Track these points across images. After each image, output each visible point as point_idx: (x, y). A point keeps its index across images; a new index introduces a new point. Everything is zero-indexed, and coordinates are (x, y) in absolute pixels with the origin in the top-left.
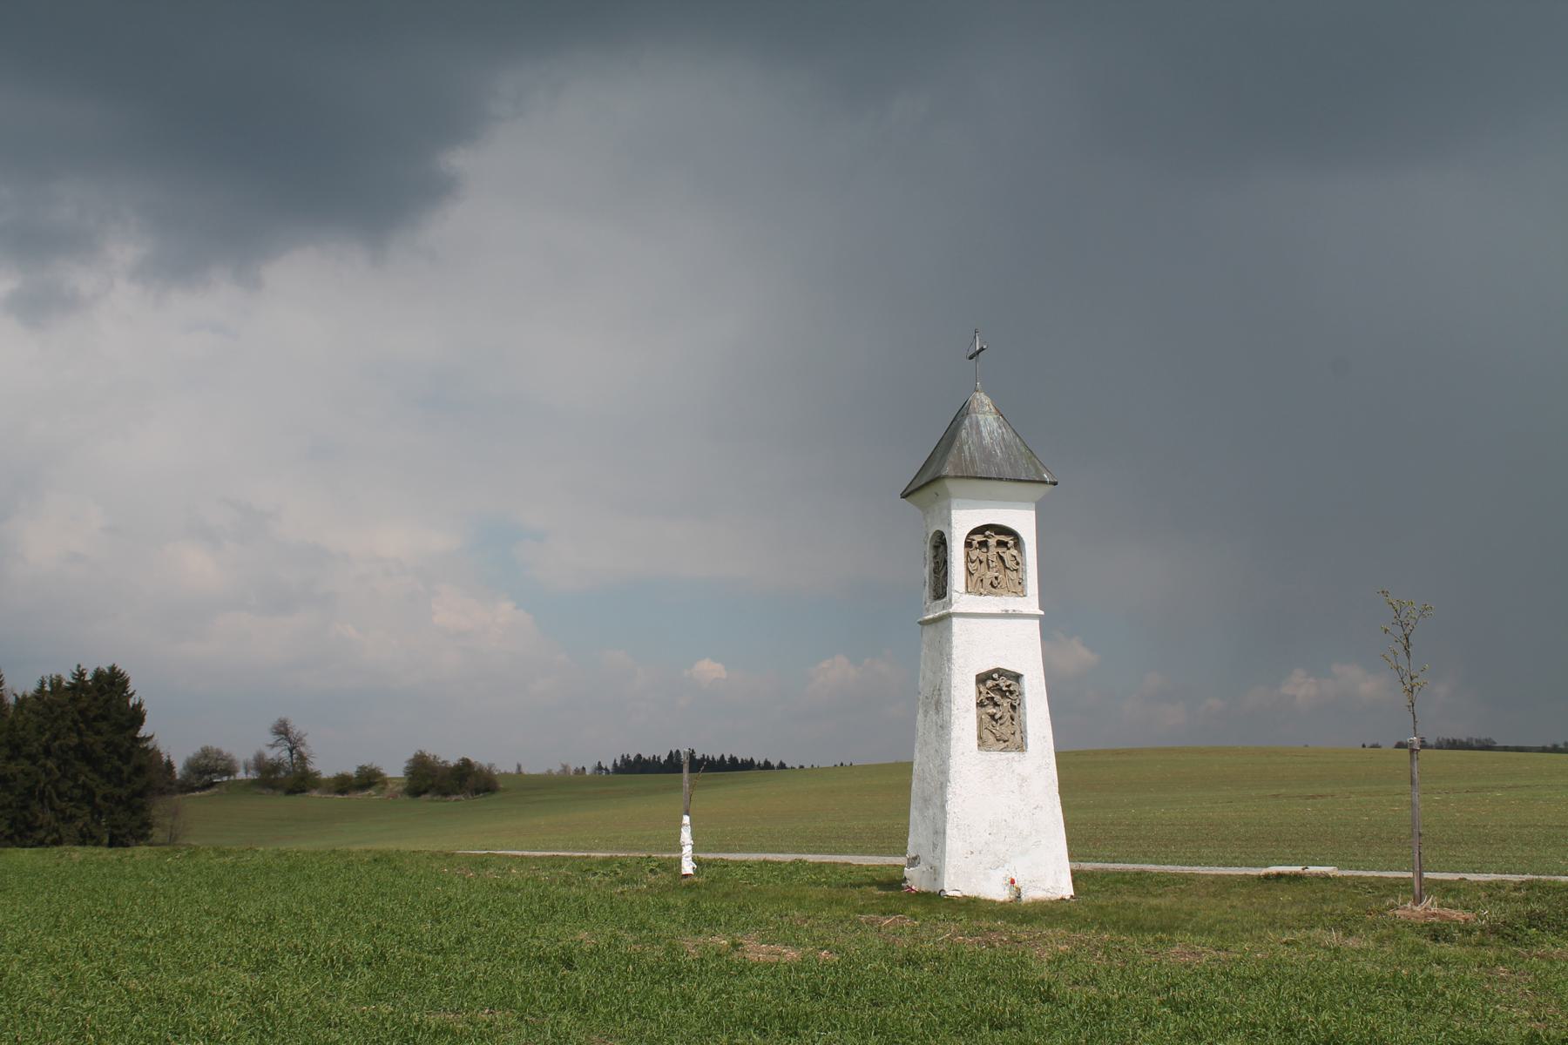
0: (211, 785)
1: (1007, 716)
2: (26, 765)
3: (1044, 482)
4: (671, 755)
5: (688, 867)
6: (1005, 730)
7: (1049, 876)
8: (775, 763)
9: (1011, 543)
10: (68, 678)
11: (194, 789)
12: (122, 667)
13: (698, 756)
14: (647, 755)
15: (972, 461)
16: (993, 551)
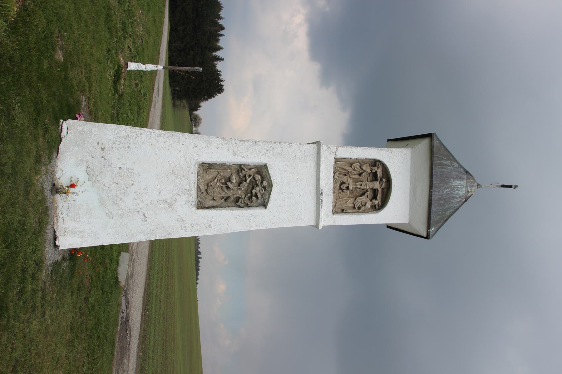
0: (192, 121)
1: (230, 193)
3: (429, 227)
6: (217, 192)
7: (78, 226)
8: (198, 282)
13: (200, 260)
15: (442, 165)
16: (369, 185)
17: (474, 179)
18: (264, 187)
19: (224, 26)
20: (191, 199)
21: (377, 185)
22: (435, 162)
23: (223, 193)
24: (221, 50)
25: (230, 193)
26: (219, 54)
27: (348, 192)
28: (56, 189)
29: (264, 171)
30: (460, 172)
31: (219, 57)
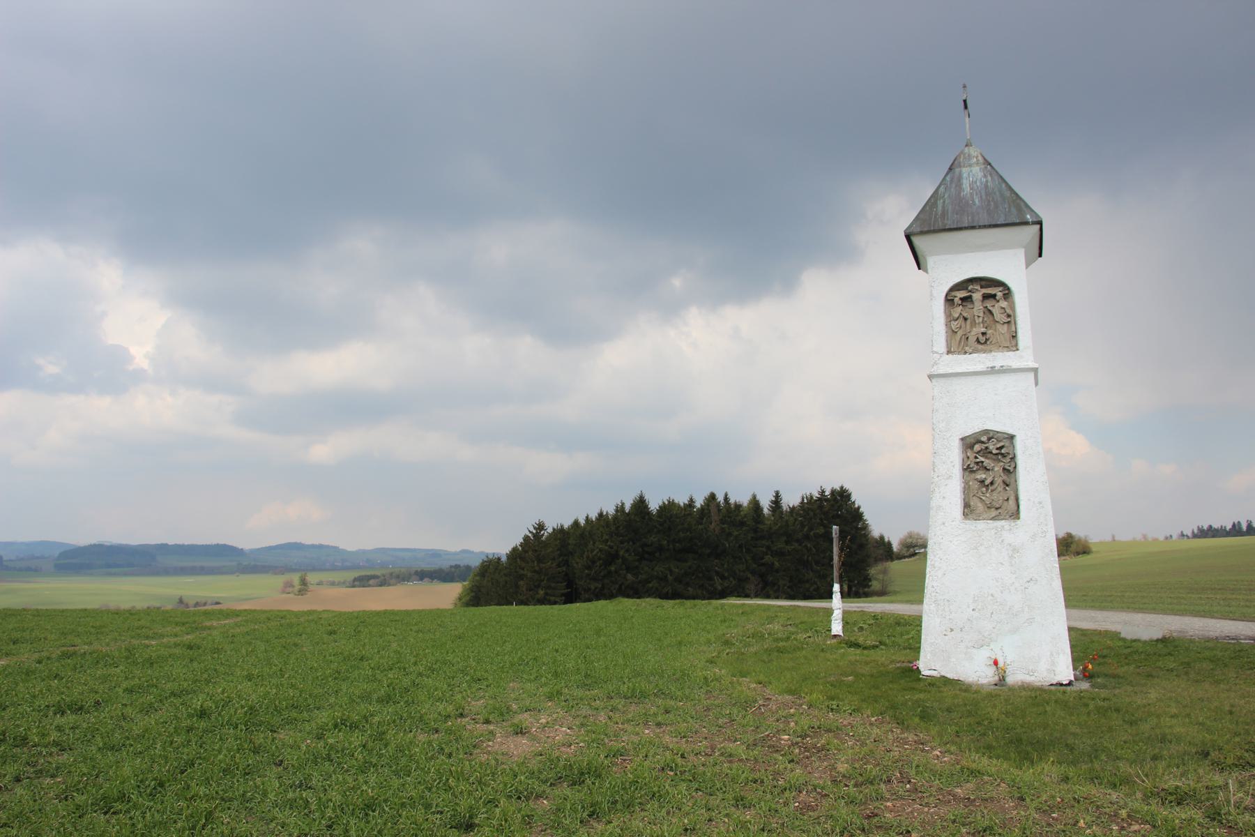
0: (914, 554)
1: (999, 481)
2: (796, 545)
3: (1026, 223)
4: (1234, 525)
5: (837, 628)
6: (997, 496)
7: (1044, 657)
9: (999, 295)
10: (816, 495)
11: (905, 557)
12: (846, 486)
14: (1216, 525)
15: (944, 214)
16: (978, 307)
17: (959, 156)
18: (989, 439)
19: (707, 494)
20: (1007, 527)
21: (977, 296)
22: (940, 225)
23: (1000, 489)
24: (758, 498)
25: (999, 481)
26: (765, 503)
27: (989, 332)
28: (1002, 681)
29: (969, 441)
30: (952, 181)
31: (772, 502)
